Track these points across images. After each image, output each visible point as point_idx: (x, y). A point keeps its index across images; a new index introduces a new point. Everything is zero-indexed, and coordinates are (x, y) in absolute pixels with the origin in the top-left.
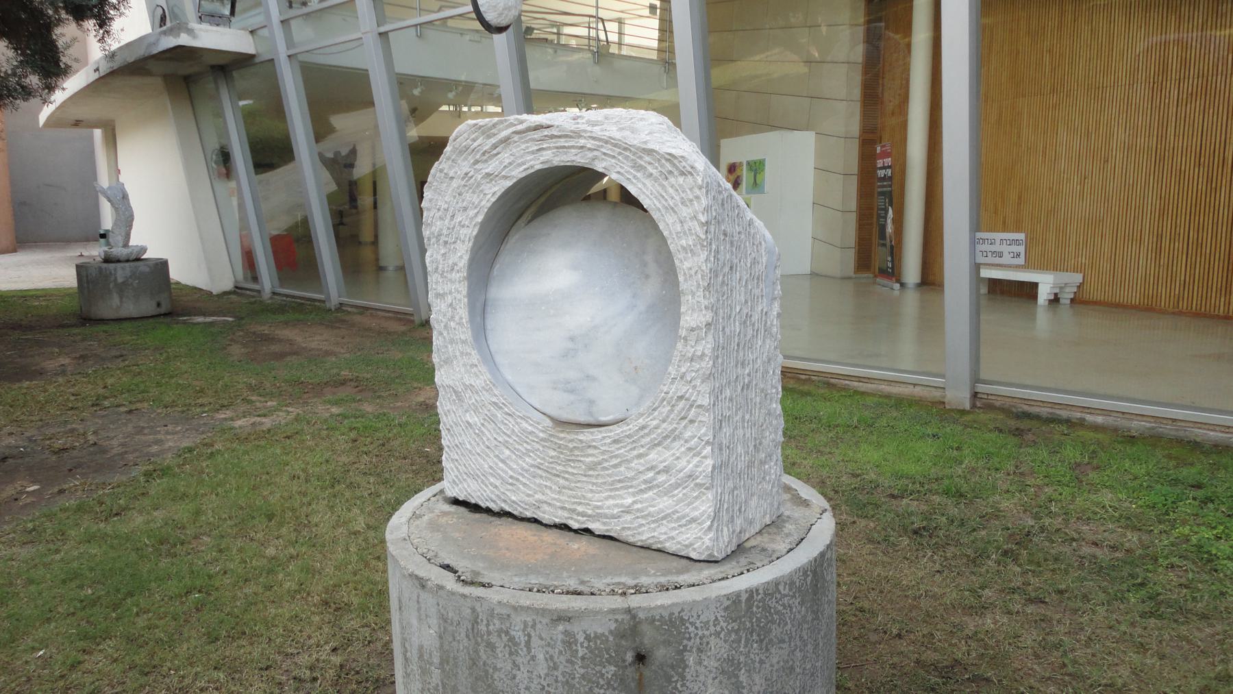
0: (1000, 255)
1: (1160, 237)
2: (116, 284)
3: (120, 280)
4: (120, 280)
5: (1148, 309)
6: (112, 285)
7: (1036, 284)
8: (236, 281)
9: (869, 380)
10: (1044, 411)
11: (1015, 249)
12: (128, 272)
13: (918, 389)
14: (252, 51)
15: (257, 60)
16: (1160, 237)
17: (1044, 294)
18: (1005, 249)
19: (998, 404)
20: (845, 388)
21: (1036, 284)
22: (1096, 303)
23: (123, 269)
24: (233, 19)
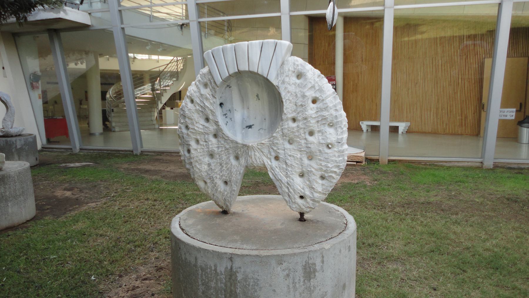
0: (506, 116)
1: (437, 109)
2: (17, 150)
3: (18, 147)
4: (18, 147)
5: (434, 133)
6: (13, 150)
7: (398, 127)
8: (43, 145)
9: (450, 162)
10: (516, 166)
11: (512, 114)
12: (23, 142)
13: (469, 163)
14: (89, 23)
15: (92, 28)
16: (437, 109)
17: (401, 130)
18: (508, 114)
19: (500, 165)
20: (442, 166)
21: (398, 127)
22: (415, 132)
23: (20, 140)
24: (81, 6)
